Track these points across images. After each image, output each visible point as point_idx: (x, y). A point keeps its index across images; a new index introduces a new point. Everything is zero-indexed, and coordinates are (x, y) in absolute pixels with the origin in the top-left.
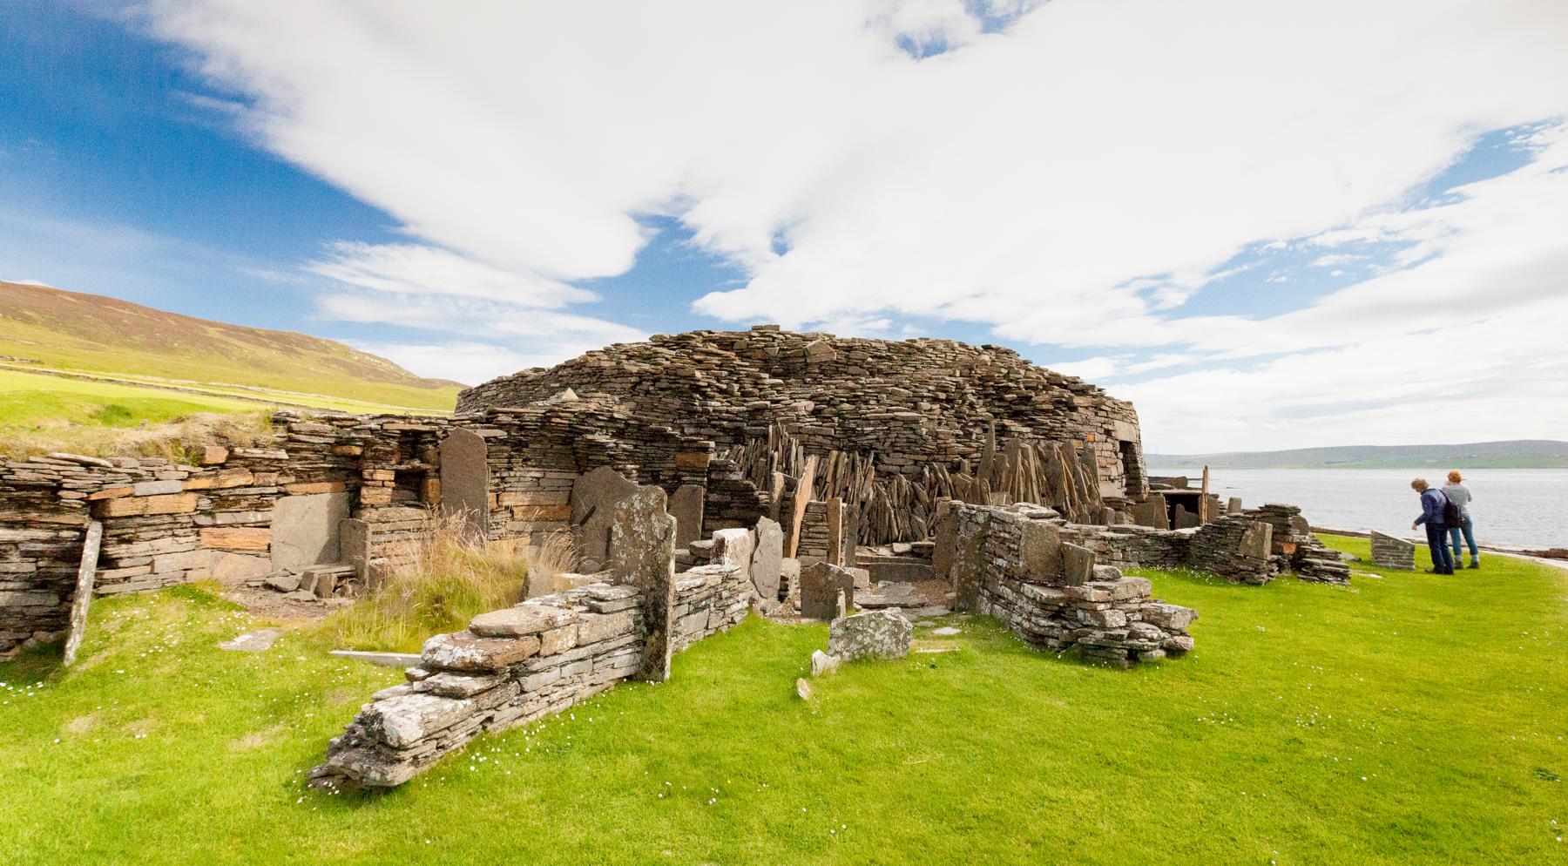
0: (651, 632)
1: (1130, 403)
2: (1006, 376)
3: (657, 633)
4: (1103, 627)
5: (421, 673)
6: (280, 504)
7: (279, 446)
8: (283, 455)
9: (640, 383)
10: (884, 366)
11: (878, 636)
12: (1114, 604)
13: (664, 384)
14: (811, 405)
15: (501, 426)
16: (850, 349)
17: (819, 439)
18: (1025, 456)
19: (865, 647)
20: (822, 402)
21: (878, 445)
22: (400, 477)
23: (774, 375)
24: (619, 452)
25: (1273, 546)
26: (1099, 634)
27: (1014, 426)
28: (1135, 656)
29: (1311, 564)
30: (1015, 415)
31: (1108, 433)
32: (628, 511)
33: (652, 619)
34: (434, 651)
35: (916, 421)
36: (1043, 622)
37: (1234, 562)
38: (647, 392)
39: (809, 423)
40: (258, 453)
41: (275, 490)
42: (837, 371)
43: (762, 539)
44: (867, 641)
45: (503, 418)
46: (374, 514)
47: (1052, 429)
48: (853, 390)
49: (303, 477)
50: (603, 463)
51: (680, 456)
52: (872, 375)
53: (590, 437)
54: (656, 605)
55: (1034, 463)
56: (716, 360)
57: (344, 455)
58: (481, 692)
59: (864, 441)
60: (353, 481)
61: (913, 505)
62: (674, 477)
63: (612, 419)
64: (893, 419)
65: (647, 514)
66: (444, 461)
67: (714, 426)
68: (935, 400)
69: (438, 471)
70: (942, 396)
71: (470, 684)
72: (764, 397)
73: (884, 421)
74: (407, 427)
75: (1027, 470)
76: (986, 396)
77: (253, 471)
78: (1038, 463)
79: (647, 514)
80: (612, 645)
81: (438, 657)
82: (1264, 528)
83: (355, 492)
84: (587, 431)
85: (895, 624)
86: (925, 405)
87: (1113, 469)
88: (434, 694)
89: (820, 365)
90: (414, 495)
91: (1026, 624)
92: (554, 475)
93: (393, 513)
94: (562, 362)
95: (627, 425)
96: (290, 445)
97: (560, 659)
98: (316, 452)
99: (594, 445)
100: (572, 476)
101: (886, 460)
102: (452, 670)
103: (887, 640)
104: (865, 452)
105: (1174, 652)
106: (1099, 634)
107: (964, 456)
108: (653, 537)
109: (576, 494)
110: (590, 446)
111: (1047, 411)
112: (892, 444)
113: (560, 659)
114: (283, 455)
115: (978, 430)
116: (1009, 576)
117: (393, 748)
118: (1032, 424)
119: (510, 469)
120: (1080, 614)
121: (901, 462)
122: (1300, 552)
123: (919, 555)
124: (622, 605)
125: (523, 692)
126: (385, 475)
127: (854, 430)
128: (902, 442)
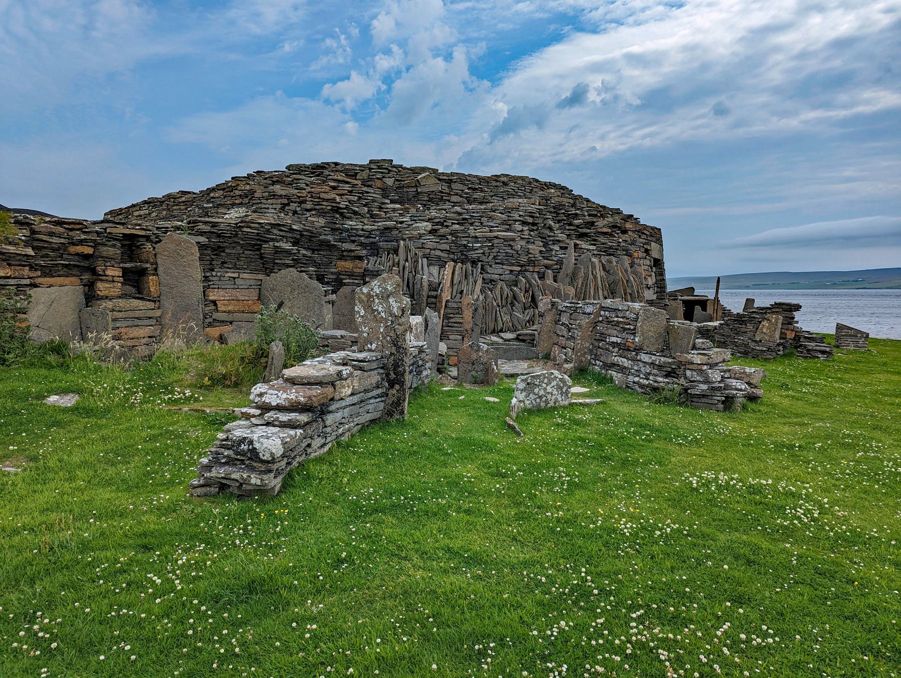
0: (392, 386)
1: (655, 234)
2: (574, 205)
3: (397, 387)
4: (707, 381)
5: (258, 412)
6: (33, 292)
7: (27, 244)
8: (30, 252)
9: (288, 204)
10: (478, 195)
11: (549, 389)
12: (712, 366)
13: (309, 206)
14: (429, 226)
15: (202, 233)
16: (450, 182)
17: (438, 253)
18: (594, 267)
19: (540, 397)
20: (437, 224)
21: (484, 258)
22: (125, 271)
23: (392, 202)
24: (301, 257)
25: (781, 333)
26: (704, 387)
27: (583, 245)
28: (728, 403)
29: (805, 346)
30: (582, 236)
31: (647, 251)
32: (369, 296)
33: (393, 376)
34: (261, 395)
35: (513, 240)
36: (660, 379)
37: (752, 345)
38: (295, 212)
39: (430, 242)
40: (12, 249)
41: (28, 282)
42: (441, 199)
43: (429, 324)
44: (542, 393)
45: (202, 227)
46: (110, 304)
47: (611, 248)
48: (460, 214)
49: (48, 272)
50: (288, 266)
51: (342, 263)
52: (469, 203)
53: (277, 244)
54: (396, 366)
55: (600, 273)
56: (347, 187)
57: (77, 254)
58: (307, 423)
59: (473, 255)
60: (86, 277)
61: (512, 304)
62: (336, 280)
63: (292, 230)
64: (496, 237)
65: (385, 296)
66: (159, 261)
67: (354, 242)
68: (524, 223)
69: (156, 269)
70: (530, 220)
71: (303, 418)
72: (390, 219)
73: (489, 240)
74: (127, 231)
75: (595, 277)
76: (559, 221)
77: (9, 265)
78: (603, 273)
79: (385, 296)
80: (370, 394)
81: (266, 399)
82: (777, 320)
83: (91, 285)
84: (273, 240)
85: (561, 380)
86: (518, 227)
87: (649, 279)
88: (274, 426)
89: (429, 194)
90: (133, 290)
91: (646, 382)
92: (245, 276)
93: (122, 303)
94: (212, 185)
95: (302, 235)
96: (36, 244)
97: (344, 403)
98: (54, 250)
99: (278, 251)
100: (260, 277)
101: (489, 269)
102: (279, 408)
103: (555, 392)
104: (474, 263)
105: (752, 398)
106: (704, 387)
107: (547, 267)
108: (392, 314)
109: (264, 292)
110: (276, 252)
111: (606, 233)
112: (495, 258)
113: (344, 403)
114: (30, 252)
115: (556, 248)
116: (624, 349)
117: (268, 462)
118: (594, 242)
119: (213, 270)
120: (688, 373)
121: (500, 271)
122: (797, 338)
123: (524, 341)
124: (374, 365)
125: (326, 427)
126: (114, 272)
127: (465, 246)
128: (501, 256)
